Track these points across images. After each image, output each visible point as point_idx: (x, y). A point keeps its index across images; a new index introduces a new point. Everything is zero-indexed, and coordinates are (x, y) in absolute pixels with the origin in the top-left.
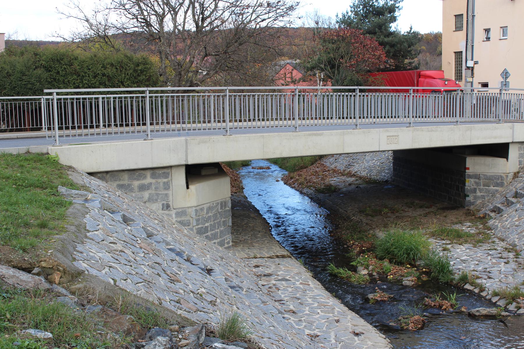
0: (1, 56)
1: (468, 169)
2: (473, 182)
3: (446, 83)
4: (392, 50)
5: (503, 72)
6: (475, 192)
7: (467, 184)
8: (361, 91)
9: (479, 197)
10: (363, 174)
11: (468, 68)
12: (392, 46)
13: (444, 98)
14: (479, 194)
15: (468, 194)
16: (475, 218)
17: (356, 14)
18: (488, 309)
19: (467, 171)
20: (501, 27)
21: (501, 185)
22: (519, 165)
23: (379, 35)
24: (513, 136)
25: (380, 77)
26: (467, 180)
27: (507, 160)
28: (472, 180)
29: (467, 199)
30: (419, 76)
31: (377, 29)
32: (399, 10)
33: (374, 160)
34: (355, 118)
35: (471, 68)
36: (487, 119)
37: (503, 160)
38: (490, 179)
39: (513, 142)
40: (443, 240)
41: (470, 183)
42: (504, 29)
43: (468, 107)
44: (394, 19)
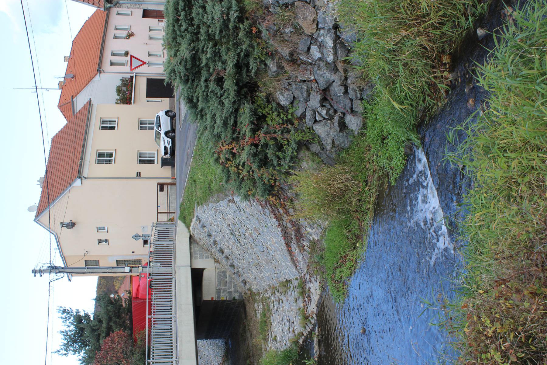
0: (87, 360)
1: (212, 298)
2: (223, 294)
3: (143, 276)
4: (114, 319)
5: (135, 239)
6: (231, 292)
7: (224, 299)
8: (149, 358)
9: (235, 289)
10: (221, 360)
11: (131, 271)
12: (110, 319)
13: (156, 291)
14: (232, 289)
15: (232, 297)
16: (251, 297)
17: (81, 348)
18: (315, 344)
19: (214, 299)
20: (97, 231)
21: (225, 273)
22: (209, 258)
23: (101, 332)
24: (185, 266)
25: (137, 335)
26: (221, 299)
27: (205, 269)
28: (222, 295)
29: (236, 298)
30: (137, 298)
31: (95, 334)
32: (79, 312)
33: (208, 349)
34: (172, 318)
35: (131, 269)
36: (174, 231)
37: (205, 272)
38: (221, 282)
39: (191, 266)
40: (268, 334)
41: (224, 297)
42: (99, 229)
43: (163, 270)
44: (87, 316)
